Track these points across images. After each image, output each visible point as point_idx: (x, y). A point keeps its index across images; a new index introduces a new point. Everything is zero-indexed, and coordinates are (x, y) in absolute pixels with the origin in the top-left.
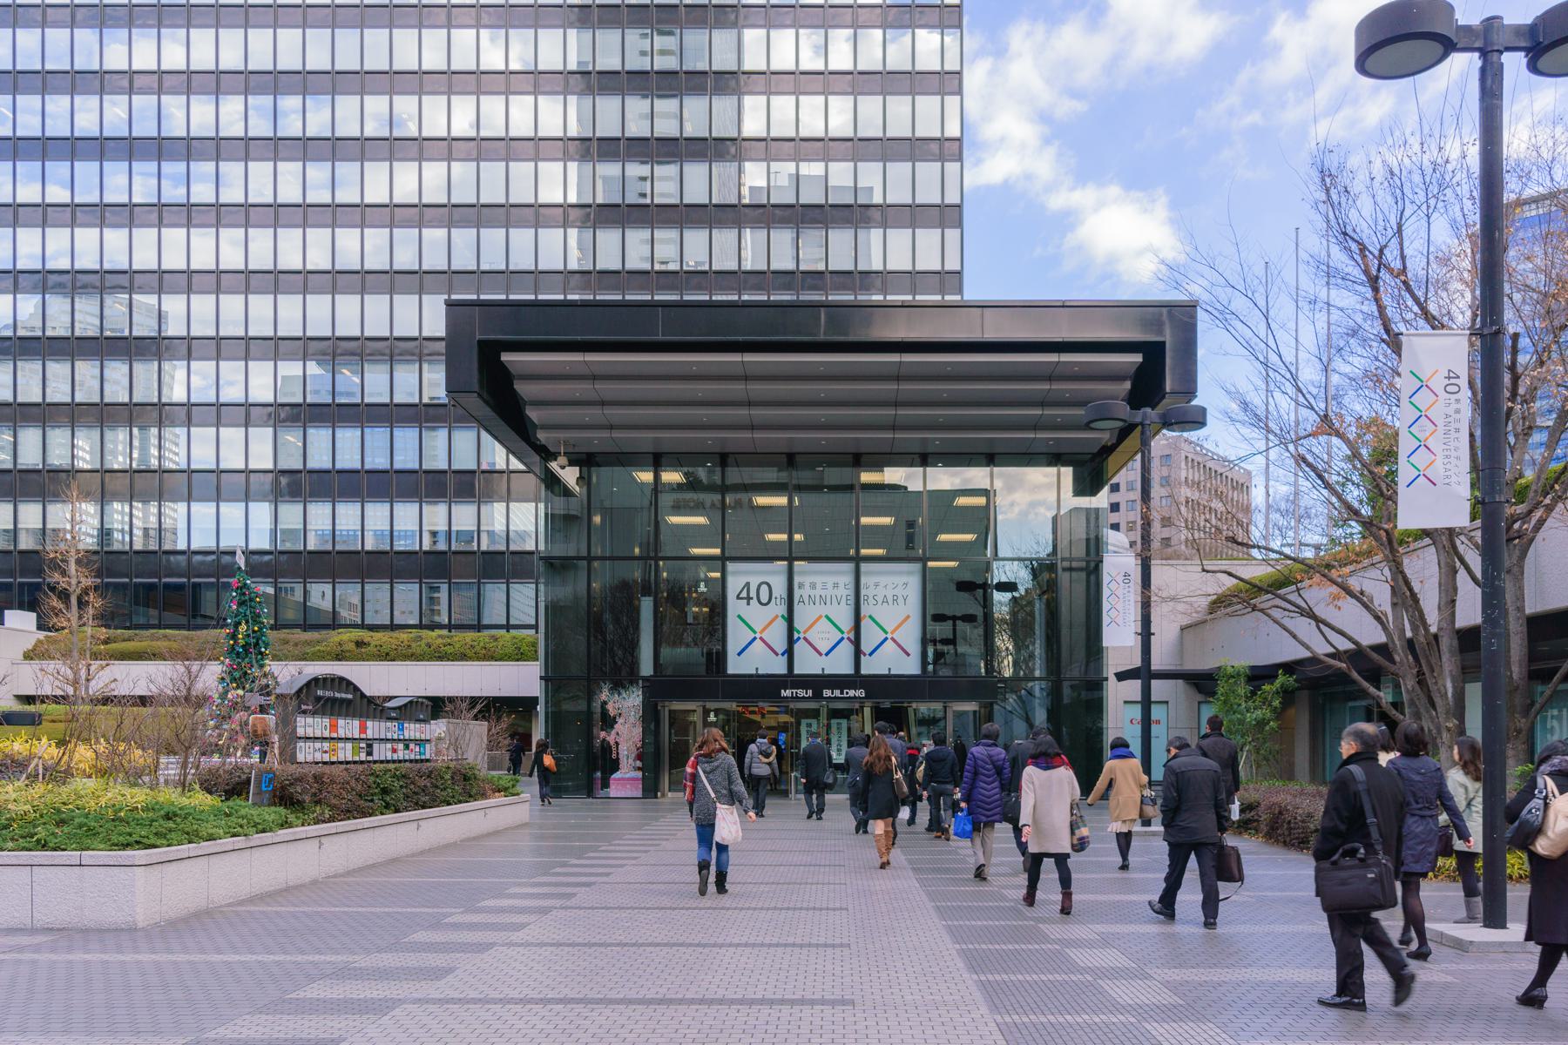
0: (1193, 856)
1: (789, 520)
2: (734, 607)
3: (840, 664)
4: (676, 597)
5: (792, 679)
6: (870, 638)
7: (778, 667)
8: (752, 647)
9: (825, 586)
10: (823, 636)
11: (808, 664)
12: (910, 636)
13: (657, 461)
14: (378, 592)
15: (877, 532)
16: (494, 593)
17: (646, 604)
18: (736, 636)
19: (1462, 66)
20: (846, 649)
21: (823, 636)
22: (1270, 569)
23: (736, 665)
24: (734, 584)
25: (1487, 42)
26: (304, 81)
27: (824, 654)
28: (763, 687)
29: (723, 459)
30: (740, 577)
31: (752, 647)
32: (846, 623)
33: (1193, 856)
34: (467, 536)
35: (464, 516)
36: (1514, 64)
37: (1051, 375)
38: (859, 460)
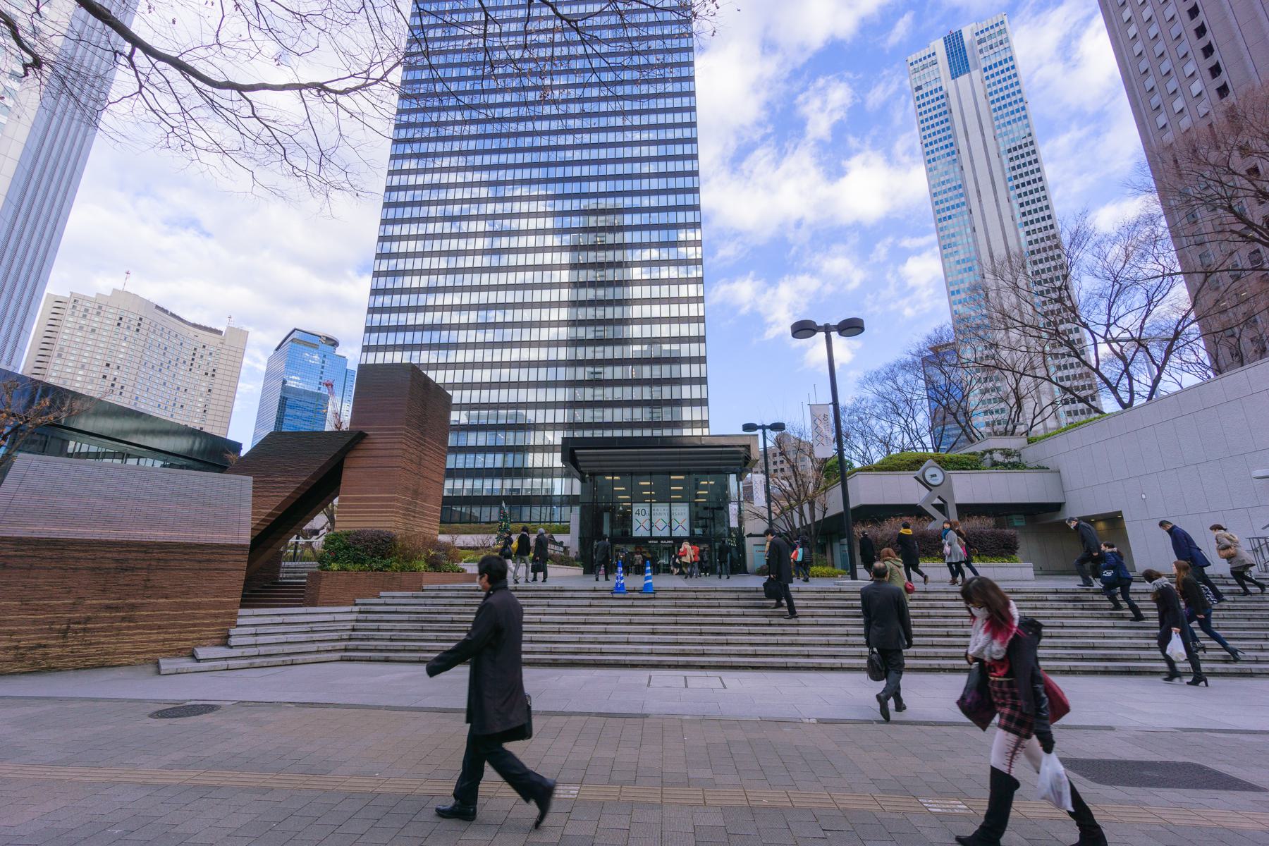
0: (486, 764)
1: (649, 488)
2: (635, 516)
3: (666, 533)
4: (612, 510)
5: (651, 538)
6: (674, 525)
7: (647, 534)
8: (640, 528)
9: (661, 510)
10: (661, 525)
11: (656, 533)
12: (686, 525)
13: (613, 474)
14: (486, 510)
15: (677, 492)
16: (526, 510)
17: (606, 517)
18: (635, 525)
19: (821, 336)
20: (667, 529)
21: (661, 525)
22: (307, 527)
23: (635, 534)
24: (635, 510)
25: (827, 329)
26: (493, 345)
27: (661, 530)
28: (643, 540)
29: (632, 474)
30: (637, 507)
31: (640, 528)
32: (667, 521)
33: (486, 764)
34: (478, 490)
35: (517, 483)
36: (834, 335)
37: (721, 453)
38: (670, 473)
